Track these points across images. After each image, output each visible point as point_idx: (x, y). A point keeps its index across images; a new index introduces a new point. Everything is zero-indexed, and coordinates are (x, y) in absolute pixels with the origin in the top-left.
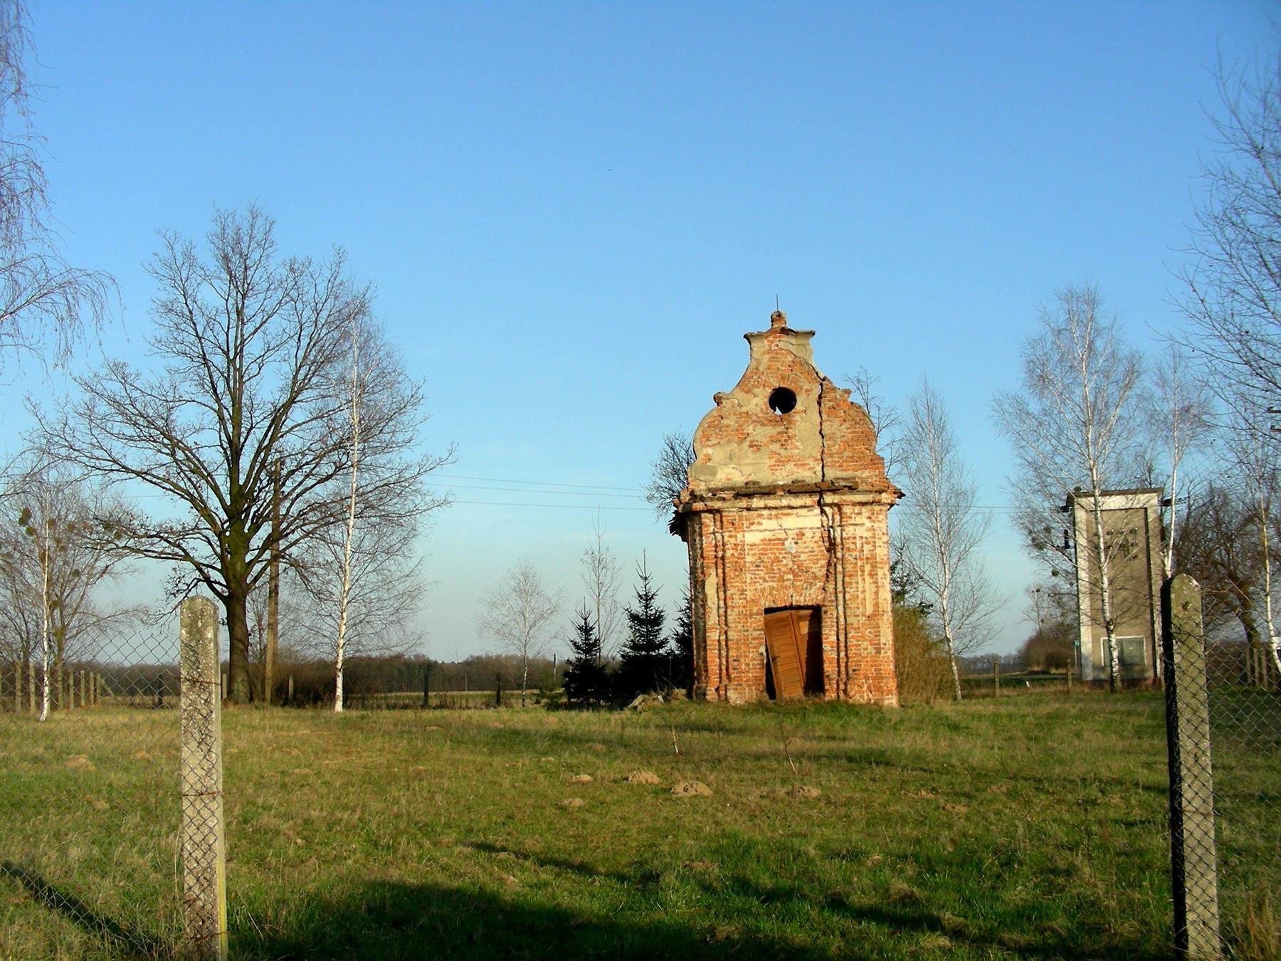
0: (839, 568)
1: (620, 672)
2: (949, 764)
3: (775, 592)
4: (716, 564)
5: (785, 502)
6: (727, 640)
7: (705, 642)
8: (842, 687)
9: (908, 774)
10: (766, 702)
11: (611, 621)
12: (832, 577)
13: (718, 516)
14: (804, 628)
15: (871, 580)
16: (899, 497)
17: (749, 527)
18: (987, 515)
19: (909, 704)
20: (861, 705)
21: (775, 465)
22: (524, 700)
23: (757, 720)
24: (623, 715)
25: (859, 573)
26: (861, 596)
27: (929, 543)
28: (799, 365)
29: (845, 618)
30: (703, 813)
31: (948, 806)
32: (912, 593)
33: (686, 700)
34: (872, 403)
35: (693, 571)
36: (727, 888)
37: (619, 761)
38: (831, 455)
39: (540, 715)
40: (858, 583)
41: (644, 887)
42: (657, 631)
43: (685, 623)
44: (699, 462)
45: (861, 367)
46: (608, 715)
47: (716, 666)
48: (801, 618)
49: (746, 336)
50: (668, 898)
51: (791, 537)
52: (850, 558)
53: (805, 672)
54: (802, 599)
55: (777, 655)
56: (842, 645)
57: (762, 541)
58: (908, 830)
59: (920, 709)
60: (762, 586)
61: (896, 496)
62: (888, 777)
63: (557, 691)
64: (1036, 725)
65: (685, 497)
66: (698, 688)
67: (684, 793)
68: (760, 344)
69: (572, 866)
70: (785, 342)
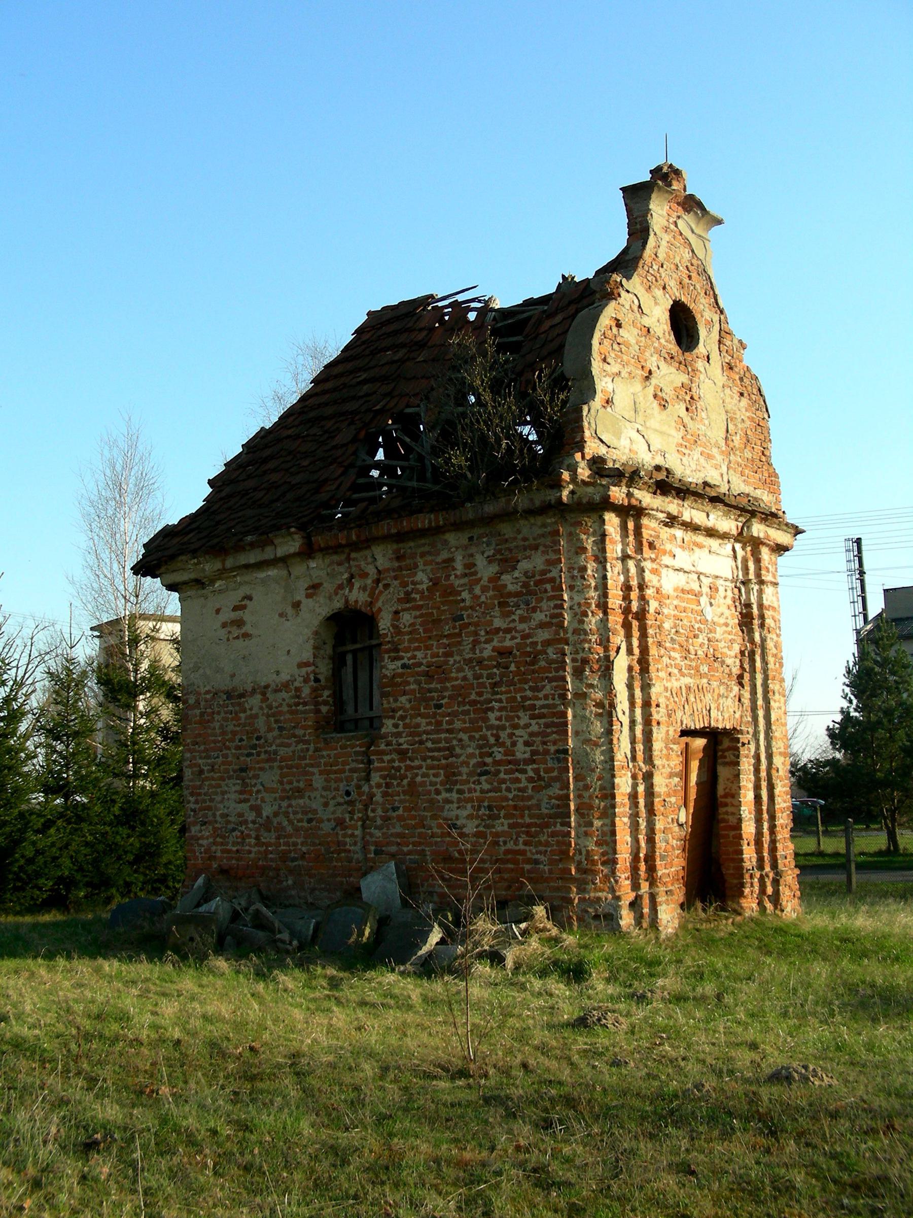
4: (627, 626)
8: (770, 890)
12: (747, 676)
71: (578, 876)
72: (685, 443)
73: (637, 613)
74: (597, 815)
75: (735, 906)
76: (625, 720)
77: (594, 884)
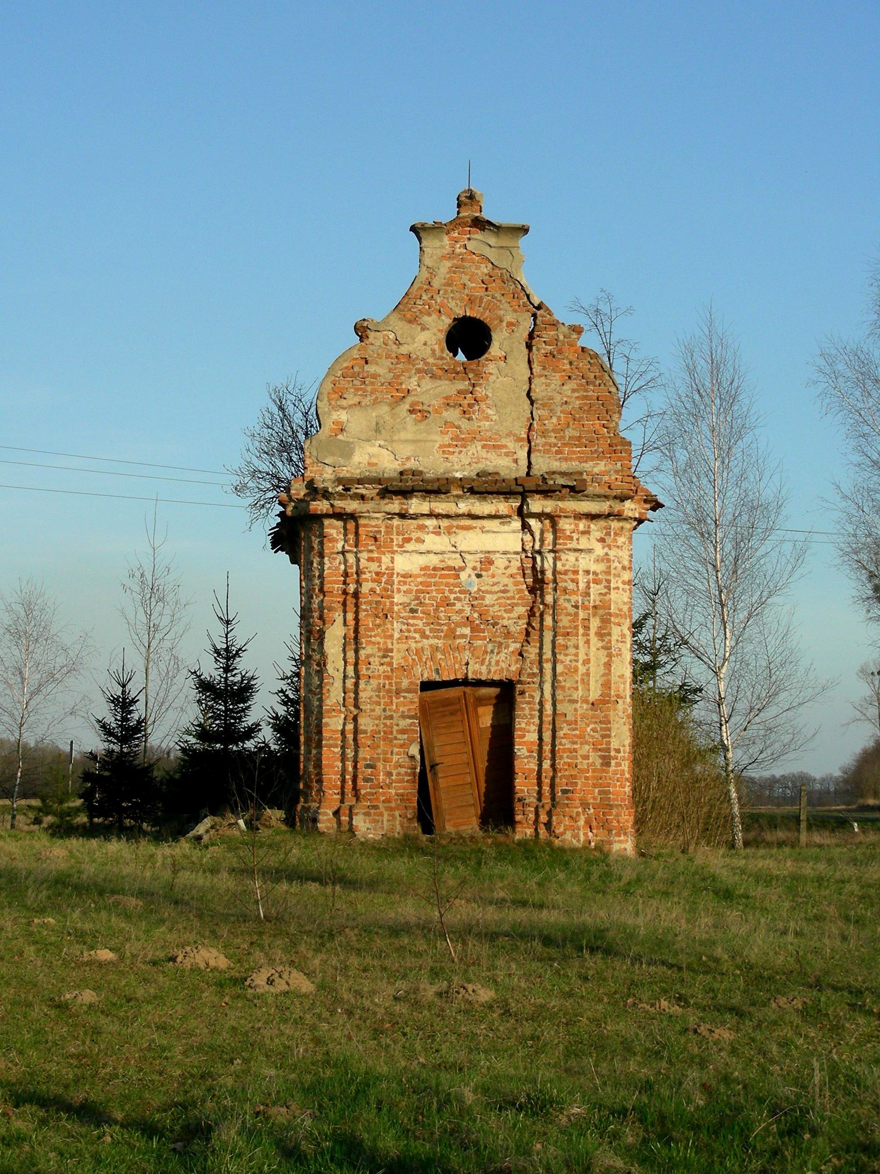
0: (548, 621)
1: (177, 776)
2: (711, 957)
3: (439, 656)
4: (344, 604)
5: (463, 507)
6: (356, 731)
7: (320, 732)
8: (543, 818)
9: (644, 970)
10: (417, 838)
11: (167, 691)
12: (534, 635)
13: (351, 525)
14: (486, 717)
15: (600, 644)
16: (654, 509)
17: (401, 546)
18: (799, 545)
19: (654, 851)
20: (574, 850)
21: (449, 445)
22: (14, 817)
23: (399, 867)
24: (178, 850)
25: (581, 631)
26: (582, 669)
27: (700, 586)
28: (498, 281)
29: (554, 705)
30: (296, 1022)
31: (703, 1029)
32: (668, 667)
33: (284, 827)
34: (617, 351)
35: (305, 614)
36: (322, 1154)
37: (163, 929)
38: (544, 434)
39: (38, 845)
40: (577, 647)
41: (185, 1147)
42: (243, 710)
43: (290, 700)
44: (325, 432)
45: (602, 291)
46: (152, 849)
47: (336, 773)
48: (480, 701)
49: (413, 229)
50: (223, 1167)
51: (470, 565)
52: (567, 605)
53: (483, 790)
54: (484, 669)
55: (437, 760)
56: (547, 748)
57: (421, 569)
58: (632, 1066)
59: (671, 861)
60: (420, 645)
61: (648, 506)
62: (608, 974)
63: (72, 805)
64: (862, 898)
65: (299, 490)
66: (306, 809)
67: (267, 987)
68: (437, 243)
69: (68, 1108)
70: (478, 241)
72: (455, 443)
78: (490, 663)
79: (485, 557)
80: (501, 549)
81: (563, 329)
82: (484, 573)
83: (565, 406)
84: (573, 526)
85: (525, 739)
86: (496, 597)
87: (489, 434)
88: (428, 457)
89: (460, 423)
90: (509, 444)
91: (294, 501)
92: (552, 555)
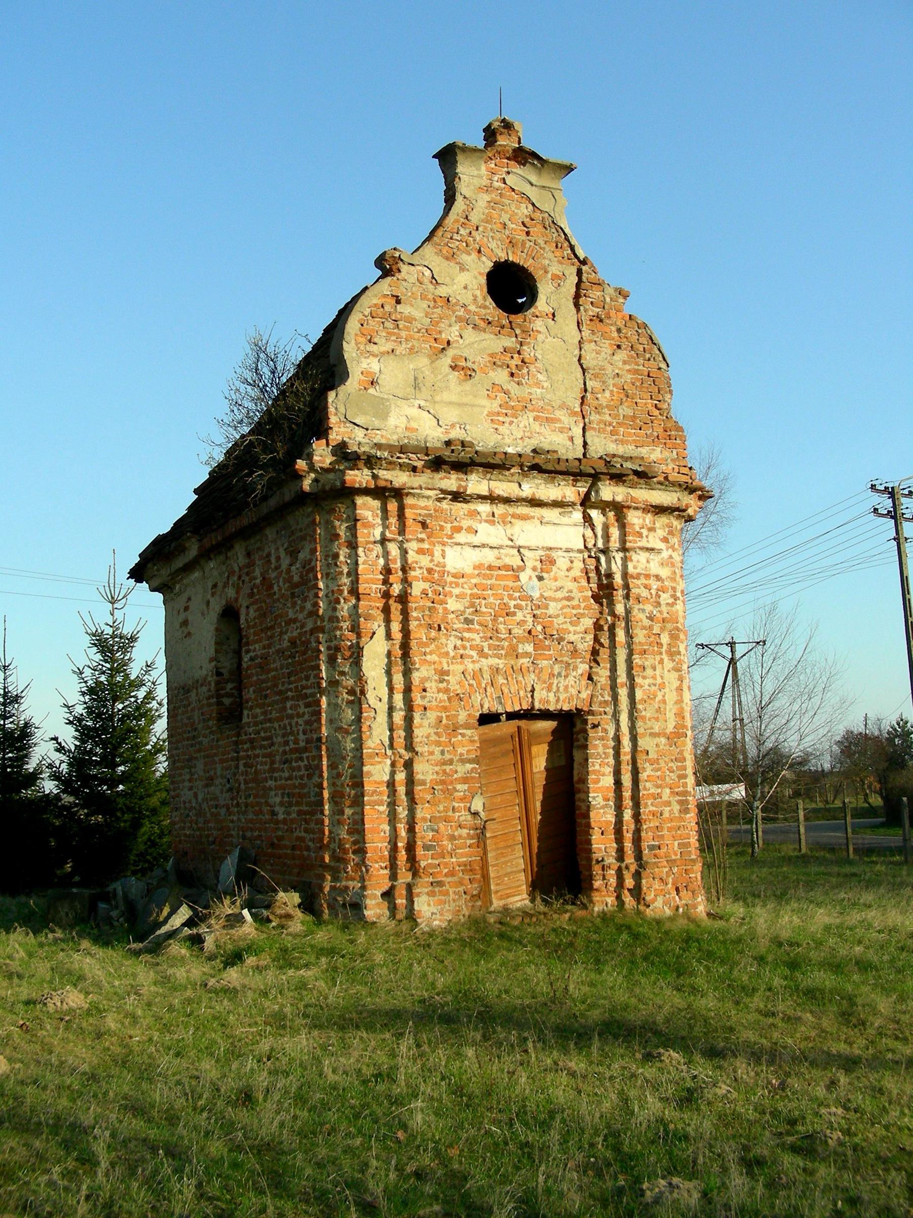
4: (386, 610)
6: (410, 782)
8: (629, 882)
12: (604, 654)
13: (393, 506)
21: (498, 414)
51: (529, 564)
56: (627, 794)
60: (477, 666)
71: (332, 864)
72: (504, 411)
73: (399, 596)
74: (348, 803)
75: (585, 901)
76: (383, 707)
77: (347, 873)
78: (558, 688)
79: (547, 556)
80: (564, 546)
81: (610, 291)
82: (545, 575)
83: (617, 379)
84: (641, 520)
85: (600, 785)
86: (560, 605)
87: (541, 403)
88: (476, 425)
89: (509, 388)
90: (563, 418)
91: (316, 471)
92: (621, 554)
